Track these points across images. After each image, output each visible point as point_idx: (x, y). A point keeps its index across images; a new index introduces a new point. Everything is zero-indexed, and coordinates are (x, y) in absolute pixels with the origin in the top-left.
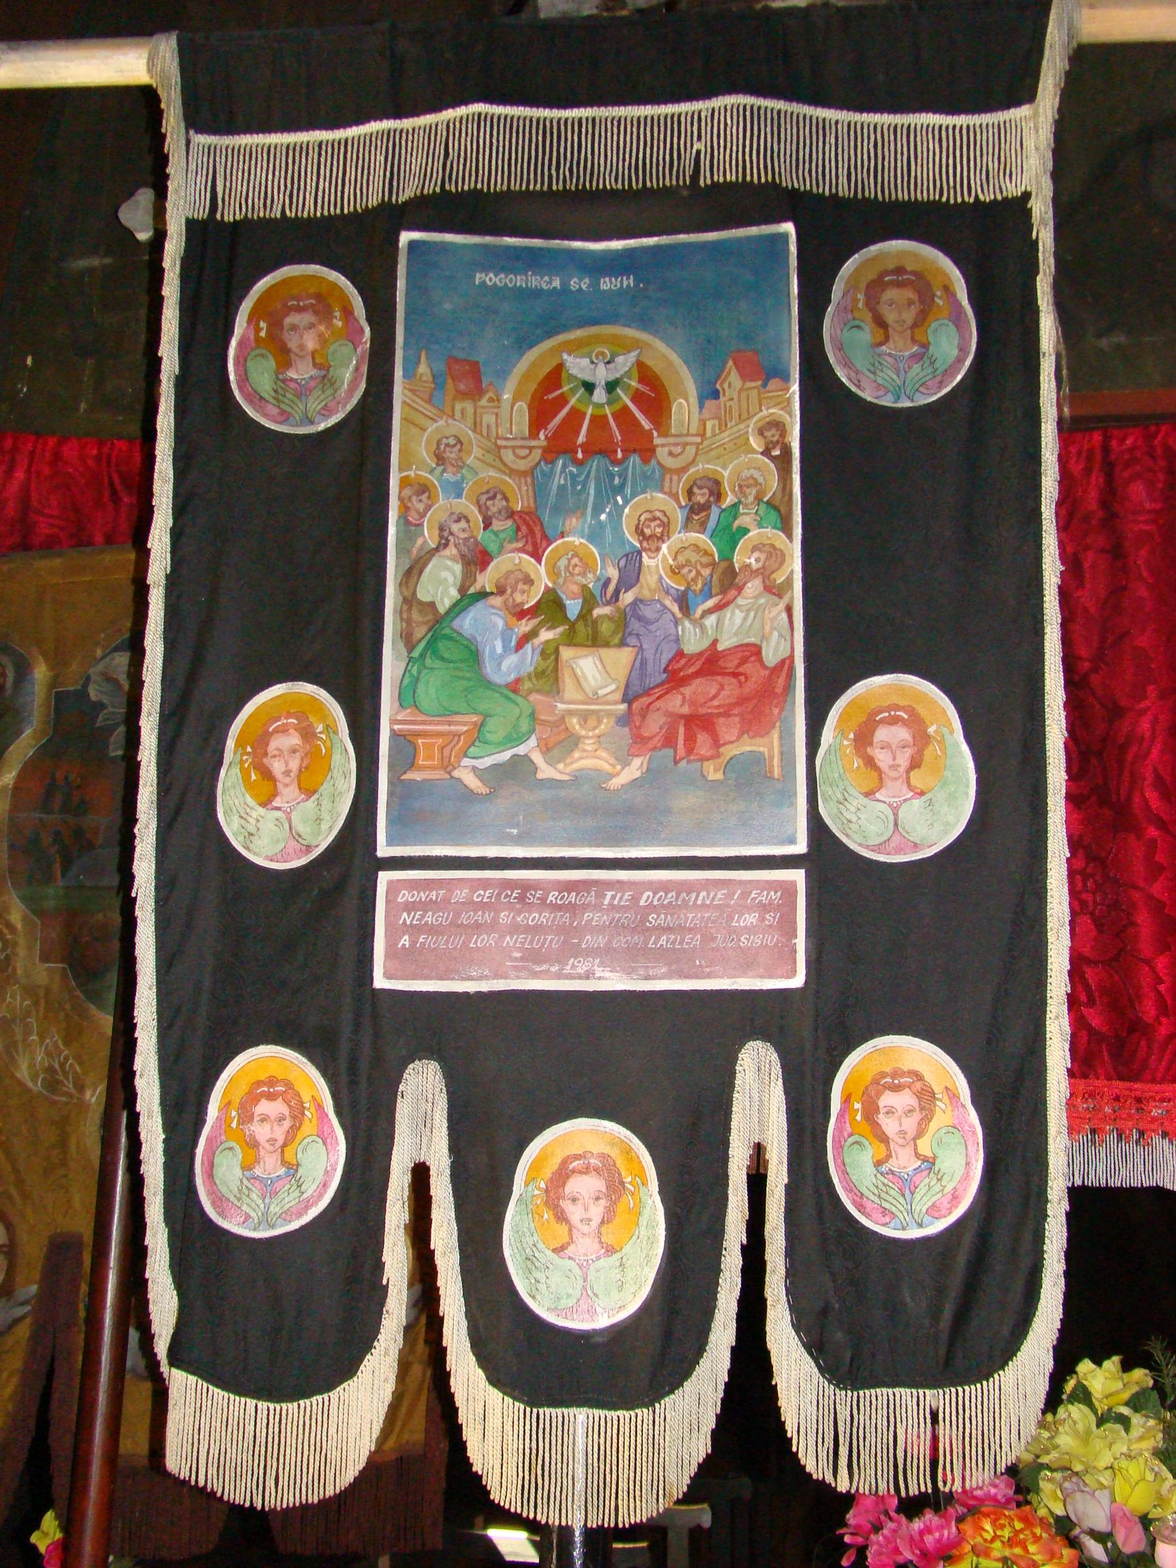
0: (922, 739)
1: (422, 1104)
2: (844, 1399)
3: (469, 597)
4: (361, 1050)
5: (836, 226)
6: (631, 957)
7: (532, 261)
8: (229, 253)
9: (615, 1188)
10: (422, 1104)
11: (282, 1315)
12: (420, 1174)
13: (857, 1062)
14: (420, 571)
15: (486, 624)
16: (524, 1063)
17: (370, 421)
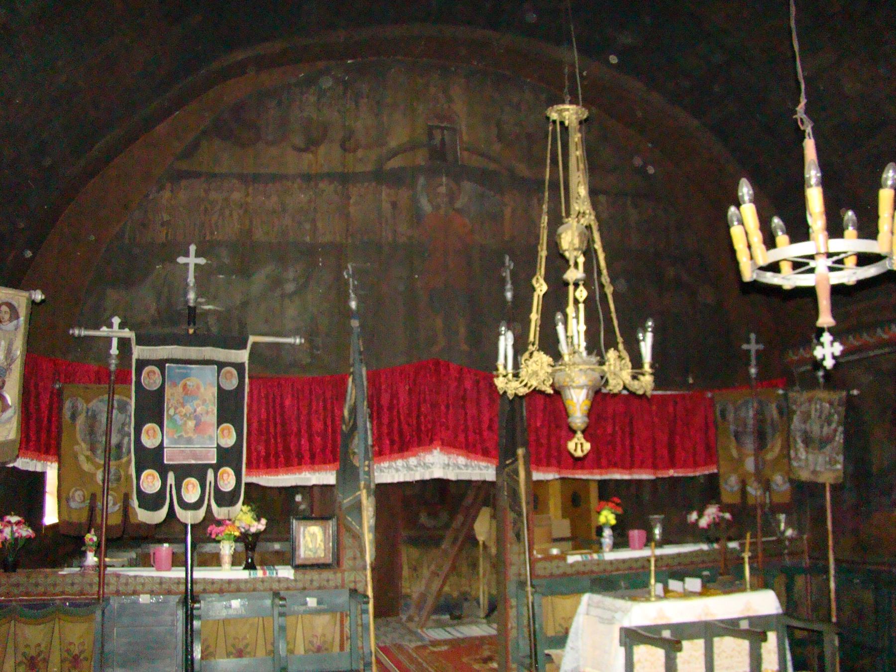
0: (229, 432)
1: (171, 478)
2: (219, 509)
3: (175, 413)
4: (163, 471)
5: (221, 365)
6: (195, 459)
7: (184, 368)
8: (142, 364)
9: (194, 486)
10: (171, 478)
11: (152, 502)
12: (171, 486)
13: (221, 471)
14: (169, 411)
15: (177, 417)
16: (183, 472)
17: (162, 387)
